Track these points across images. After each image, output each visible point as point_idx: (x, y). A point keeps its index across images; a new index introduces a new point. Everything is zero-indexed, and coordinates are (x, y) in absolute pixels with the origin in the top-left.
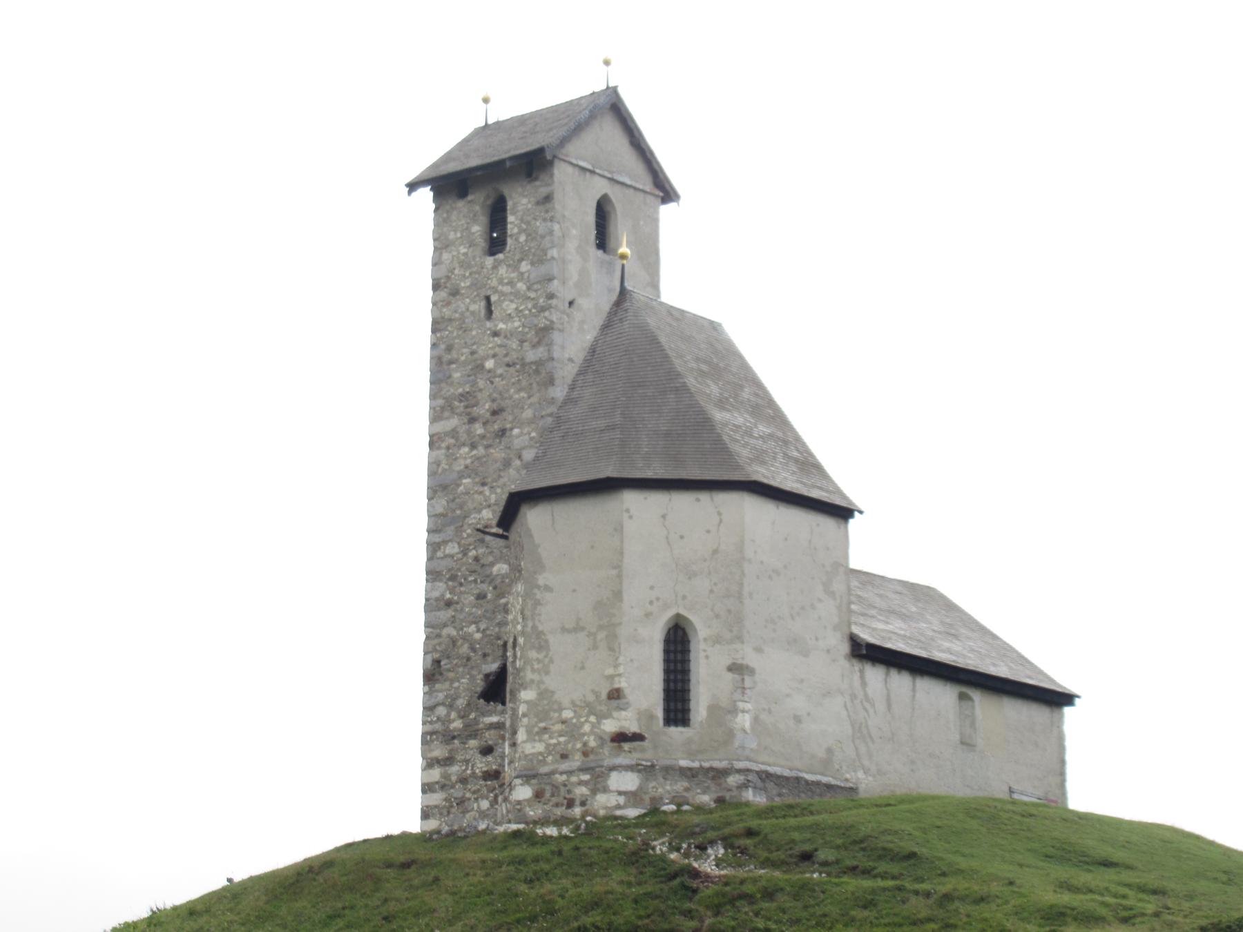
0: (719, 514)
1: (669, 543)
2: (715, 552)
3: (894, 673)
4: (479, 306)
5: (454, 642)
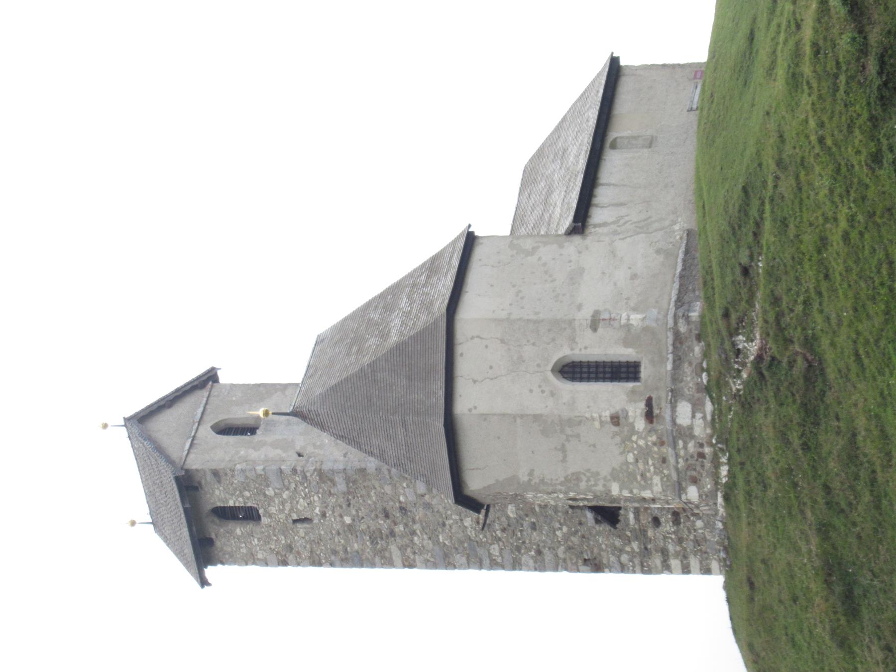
0: (472, 338)
2: (502, 341)
3: (595, 201)
4: (301, 528)
5: (570, 548)
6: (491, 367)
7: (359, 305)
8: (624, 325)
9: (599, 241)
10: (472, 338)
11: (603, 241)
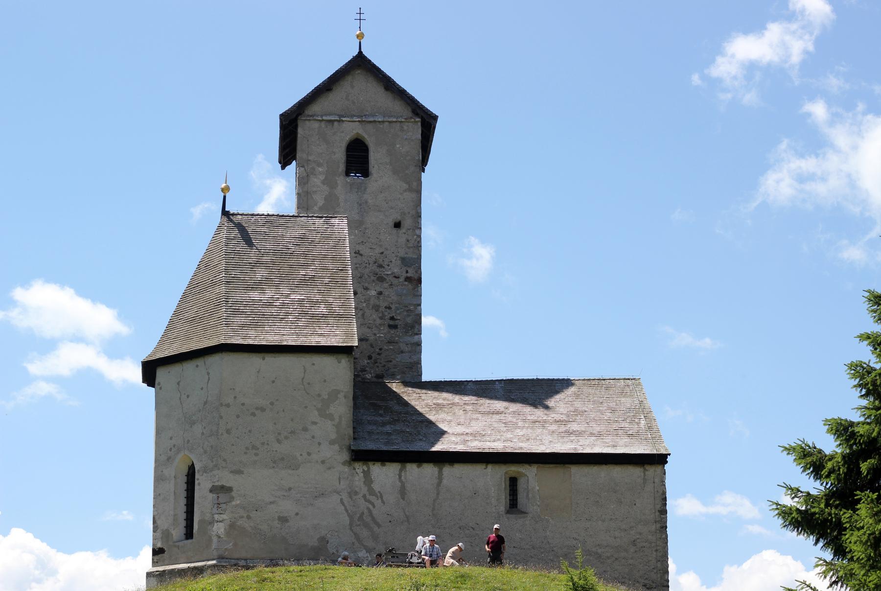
0: (208, 374)
1: (181, 404)
2: (205, 403)
3: (647, 467)
6: (188, 396)
7: (422, 251)
8: (213, 518)
9: (339, 479)
10: (208, 374)
11: (340, 483)
